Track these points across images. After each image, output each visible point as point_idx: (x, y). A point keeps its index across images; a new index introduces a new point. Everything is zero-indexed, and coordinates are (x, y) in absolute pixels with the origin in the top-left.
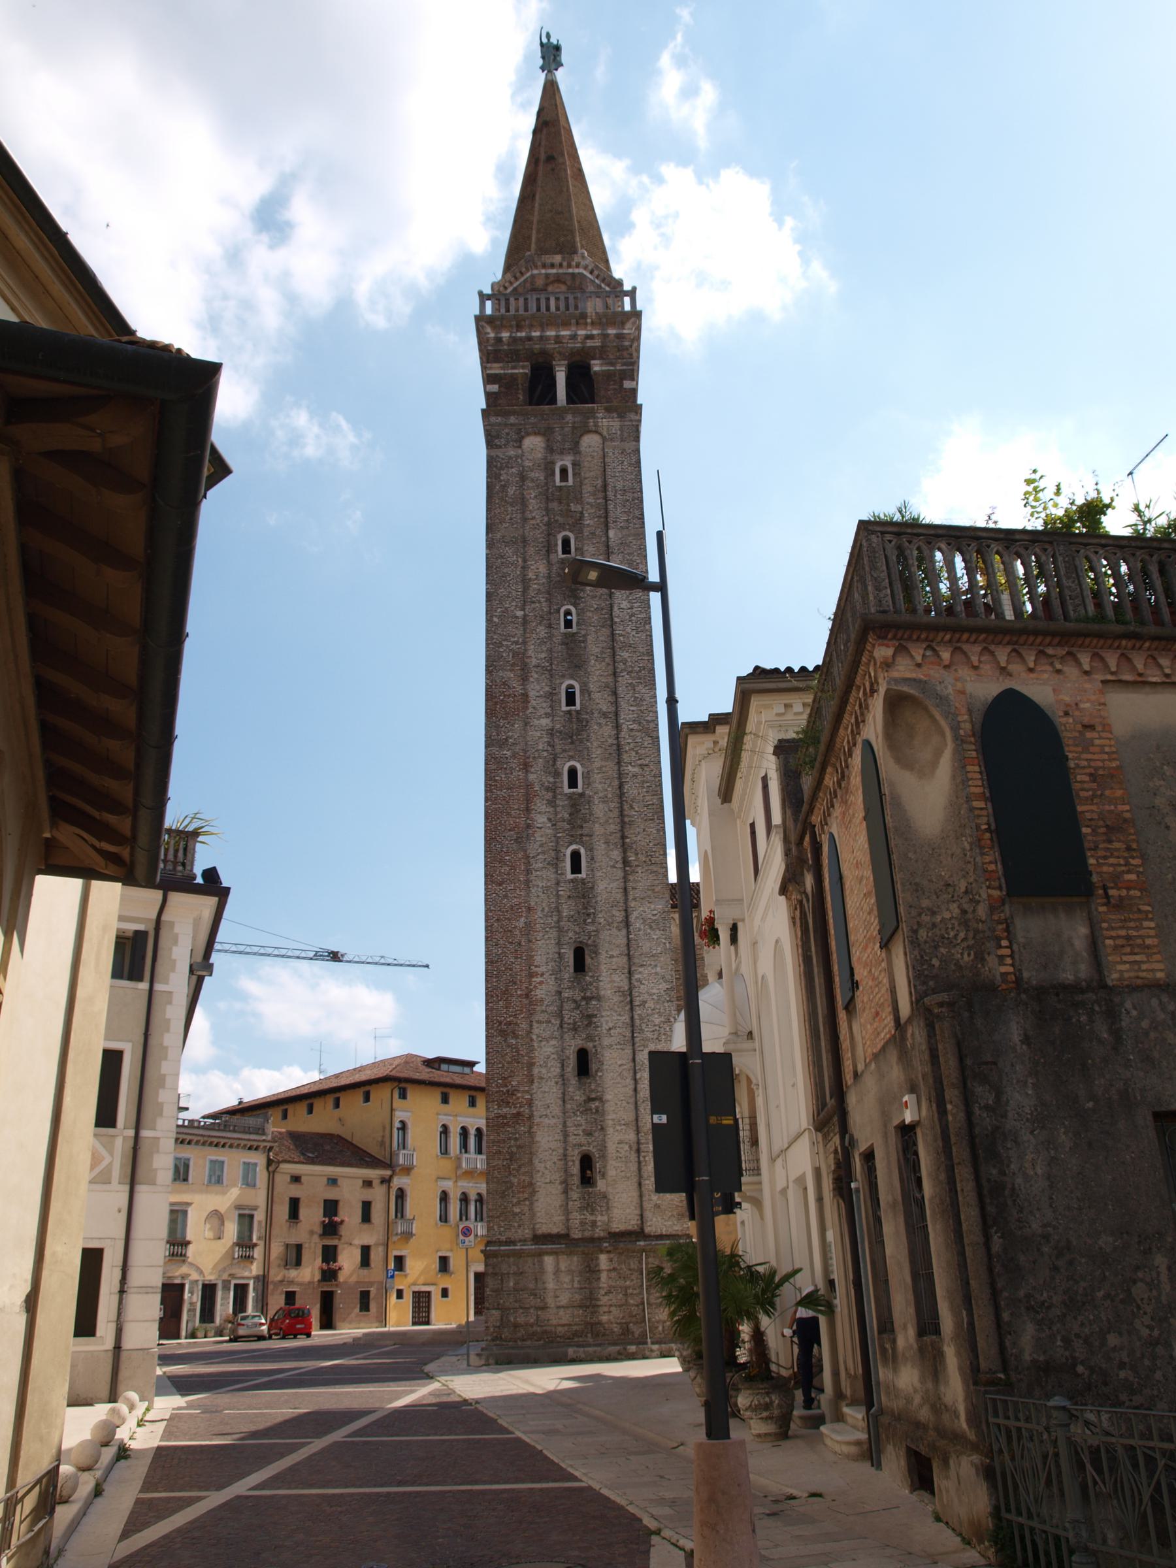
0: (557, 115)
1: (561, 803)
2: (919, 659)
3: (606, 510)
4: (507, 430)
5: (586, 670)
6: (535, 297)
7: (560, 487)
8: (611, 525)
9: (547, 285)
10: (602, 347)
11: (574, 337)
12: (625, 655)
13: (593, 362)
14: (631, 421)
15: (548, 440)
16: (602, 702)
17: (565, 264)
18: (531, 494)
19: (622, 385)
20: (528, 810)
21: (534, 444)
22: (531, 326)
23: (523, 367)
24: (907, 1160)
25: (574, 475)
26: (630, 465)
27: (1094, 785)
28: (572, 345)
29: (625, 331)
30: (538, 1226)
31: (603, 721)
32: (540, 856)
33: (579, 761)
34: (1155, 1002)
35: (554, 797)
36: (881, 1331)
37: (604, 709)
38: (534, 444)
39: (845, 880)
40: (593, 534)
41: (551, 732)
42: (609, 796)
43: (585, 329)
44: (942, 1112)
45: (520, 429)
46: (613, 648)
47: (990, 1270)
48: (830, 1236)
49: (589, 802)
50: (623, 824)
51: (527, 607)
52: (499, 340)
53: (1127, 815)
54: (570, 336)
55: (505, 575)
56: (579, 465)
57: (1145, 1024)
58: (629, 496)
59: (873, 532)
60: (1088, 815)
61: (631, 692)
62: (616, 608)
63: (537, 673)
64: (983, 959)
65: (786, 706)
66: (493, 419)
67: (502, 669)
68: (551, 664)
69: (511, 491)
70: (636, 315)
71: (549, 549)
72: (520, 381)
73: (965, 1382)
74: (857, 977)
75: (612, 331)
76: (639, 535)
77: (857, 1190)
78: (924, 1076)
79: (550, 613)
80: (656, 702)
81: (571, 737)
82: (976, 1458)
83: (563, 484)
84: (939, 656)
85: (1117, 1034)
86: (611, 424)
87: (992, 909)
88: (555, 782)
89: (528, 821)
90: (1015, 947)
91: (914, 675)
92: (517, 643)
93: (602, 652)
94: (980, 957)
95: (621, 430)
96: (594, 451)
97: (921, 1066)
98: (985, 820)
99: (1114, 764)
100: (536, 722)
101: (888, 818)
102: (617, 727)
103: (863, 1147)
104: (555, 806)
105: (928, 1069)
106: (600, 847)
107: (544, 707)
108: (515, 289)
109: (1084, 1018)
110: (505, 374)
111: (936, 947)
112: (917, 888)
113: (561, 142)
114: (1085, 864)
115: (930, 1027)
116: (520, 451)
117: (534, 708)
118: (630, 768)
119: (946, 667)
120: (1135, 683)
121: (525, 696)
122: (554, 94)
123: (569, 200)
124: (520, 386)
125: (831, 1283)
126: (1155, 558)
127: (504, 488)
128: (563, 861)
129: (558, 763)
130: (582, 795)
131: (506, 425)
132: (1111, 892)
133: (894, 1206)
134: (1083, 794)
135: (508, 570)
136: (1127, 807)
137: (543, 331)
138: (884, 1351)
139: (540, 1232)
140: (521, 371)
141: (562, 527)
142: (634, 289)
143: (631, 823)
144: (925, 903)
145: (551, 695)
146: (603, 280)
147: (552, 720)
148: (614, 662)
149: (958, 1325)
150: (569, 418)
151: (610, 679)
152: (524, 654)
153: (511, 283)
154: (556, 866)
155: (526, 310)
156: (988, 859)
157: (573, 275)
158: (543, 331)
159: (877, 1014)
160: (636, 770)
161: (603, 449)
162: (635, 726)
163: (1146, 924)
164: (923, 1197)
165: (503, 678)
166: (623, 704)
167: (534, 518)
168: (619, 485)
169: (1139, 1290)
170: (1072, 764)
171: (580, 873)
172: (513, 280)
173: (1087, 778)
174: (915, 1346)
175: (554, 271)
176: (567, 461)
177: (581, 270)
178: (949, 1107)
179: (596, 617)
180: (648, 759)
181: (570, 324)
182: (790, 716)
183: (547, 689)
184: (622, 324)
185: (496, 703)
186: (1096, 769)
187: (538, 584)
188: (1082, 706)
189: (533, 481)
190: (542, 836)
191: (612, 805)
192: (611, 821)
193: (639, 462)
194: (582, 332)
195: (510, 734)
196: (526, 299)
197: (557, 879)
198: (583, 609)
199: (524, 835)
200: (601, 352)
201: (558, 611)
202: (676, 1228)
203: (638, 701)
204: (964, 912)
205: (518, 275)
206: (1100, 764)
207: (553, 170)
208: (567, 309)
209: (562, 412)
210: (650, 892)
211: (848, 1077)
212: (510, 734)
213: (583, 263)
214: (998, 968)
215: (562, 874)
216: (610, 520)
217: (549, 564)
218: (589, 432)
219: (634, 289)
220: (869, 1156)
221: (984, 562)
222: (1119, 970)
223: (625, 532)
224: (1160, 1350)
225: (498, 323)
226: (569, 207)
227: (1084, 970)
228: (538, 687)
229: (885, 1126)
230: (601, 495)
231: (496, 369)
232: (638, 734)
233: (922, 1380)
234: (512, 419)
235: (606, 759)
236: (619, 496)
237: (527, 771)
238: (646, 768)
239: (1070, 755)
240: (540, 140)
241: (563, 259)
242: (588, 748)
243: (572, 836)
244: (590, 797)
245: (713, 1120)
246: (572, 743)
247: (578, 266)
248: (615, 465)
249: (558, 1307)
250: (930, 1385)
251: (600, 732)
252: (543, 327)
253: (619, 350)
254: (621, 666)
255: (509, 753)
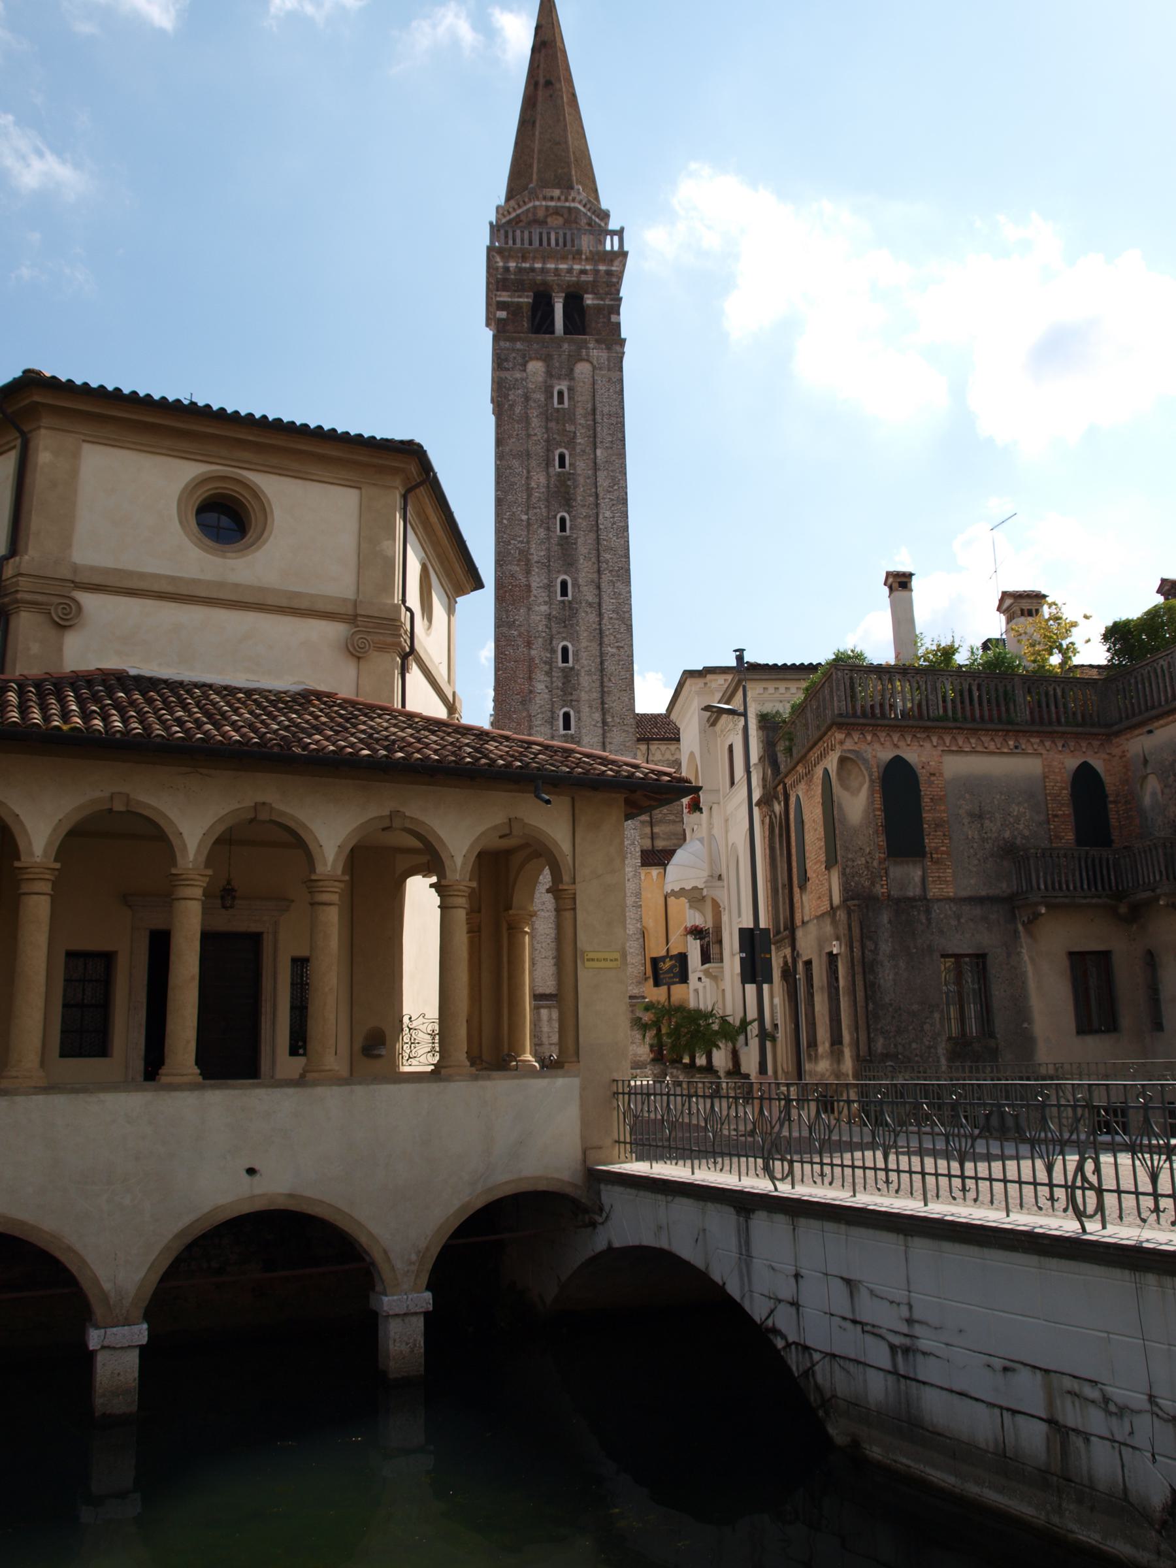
0: (554, 34)
1: (556, 675)
2: (856, 740)
3: (595, 430)
4: (514, 355)
5: (576, 567)
6: (538, 231)
7: (558, 409)
8: (598, 445)
9: (546, 217)
10: (594, 281)
11: (570, 271)
12: (608, 556)
13: (586, 296)
14: (617, 353)
15: (548, 366)
16: (589, 594)
17: (563, 198)
18: (534, 413)
19: (610, 319)
20: (530, 678)
21: (536, 367)
22: (534, 259)
23: (527, 297)
24: (830, 968)
25: (569, 398)
26: (615, 392)
27: (932, 804)
28: (569, 279)
29: (614, 268)
30: (535, 988)
31: (589, 610)
32: (539, 716)
33: (570, 642)
34: (947, 906)
35: (551, 669)
36: (809, 1046)
37: (590, 600)
38: (536, 367)
39: (805, 823)
40: (584, 451)
41: (549, 617)
42: (593, 670)
43: (580, 264)
44: (852, 951)
45: (525, 355)
46: (598, 550)
47: (867, 1017)
48: (777, 1001)
49: (577, 675)
50: (603, 693)
51: (530, 512)
52: (507, 269)
53: (945, 819)
54: (567, 269)
55: (514, 484)
56: (573, 390)
57: (942, 916)
58: (613, 420)
59: (839, 670)
60: (927, 819)
61: (611, 587)
62: (601, 517)
63: (538, 568)
64: (874, 885)
65: (765, 689)
66: (502, 344)
67: (510, 564)
68: (549, 561)
69: (518, 410)
70: (623, 254)
71: (548, 463)
72: (525, 310)
73: (853, 1061)
74: (808, 875)
75: (602, 268)
76: (620, 455)
77: (800, 979)
78: (844, 935)
79: (549, 518)
80: (630, 596)
81: (564, 622)
82: (856, 1090)
83: (560, 406)
84: (866, 738)
85: (929, 920)
86: (600, 354)
87: (880, 863)
88: (552, 658)
89: (531, 688)
90: (889, 881)
91: (853, 748)
92: (522, 542)
93: (589, 553)
94: (873, 884)
95: (609, 360)
96: (585, 378)
97: (842, 930)
98: (880, 821)
99: (942, 793)
100: (537, 608)
101: (835, 812)
102: (600, 615)
103: (805, 958)
104: (551, 677)
105: (846, 932)
106: (585, 710)
107: (543, 596)
108: (518, 216)
109: (916, 913)
110: (512, 303)
111: (853, 877)
112: (847, 849)
113: (558, 66)
114: (923, 842)
115: (849, 914)
116: (525, 375)
117: (535, 596)
118: (609, 649)
119: (869, 744)
120: (957, 751)
121: (529, 586)
122: (551, 12)
123: (565, 130)
124: (525, 315)
125: (776, 1026)
126: (976, 682)
127: (512, 406)
128: (558, 720)
129: (554, 642)
130: (572, 669)
131: (513, 350)
132: (934, 856)
133: (822, 988)
134: (926, 808)
135: (515, 480)
136: (945, 815)
137: (544, 263)
138: (809, 1056)
139: (537, 992)
140: (526, 300)
141: (559, 445)
142: (622, 229)
143: (609, 693)
144: (850, 856)
145: (549, 587)
146: (594, 213)
147: (550, 608)
148: (599, 562)
149: (852, 1039)
150: (566, 346)
151: (595, 575)
152: (527, 551)
153: (514, 210)
154: (552, 724)
155: (531, 244)
156: (880, 839)
157: (569, 209)
158: (544, 263)
159: (820, 898)
160: (614, 650)
161: (593, 377)
162: (614, 616)
163: (948, 871)
164: (838, 986)
165: (511, 571)
166: (605, 597)
167: (535, 435)
168: (606, 410)
169: (927, 1027)
170: (922, 793)
171: (570, 730)
172: (516, 207)
173: (929, 800)
174: (829, 1051)
175: (552, 204)
176: (563, 386)
177: (576, 205)
178: (855, 950)
179: (585, 523)
180: (623, 642)
181: (567, 258)
182: (766, 695)
183: (546, 581)
184: (611, 262)
185: (506, 591)
186: (933, 796)
187: (539, 493)
188: (931, 763)
189: (535, 401)
190: (541, 700)
191: (595, 677)
192: (594, 690)
193: (622, 390)
194: (577, 267)
195: (517, 617)
196: (530, 233)
197: (552, 733)
198: (574, 516)
199: (528, 698)
200: (593, 287)
201: (555, 517)
202: (634, 991)
203: (617, 595)
204: (867, 862)
205: (521, 203)
206: (936, 793)
207: (551, 96)
208: (565, 245)
209: (560, 340)
210: (622, 747)
211: (798, 922)
212: (517, 617)
213: (578, 198)
214: (880, 890)
215: (556, 730)
216: (598, 440)
217: (548, 476)
218: (582, 360)
219: (622, 229)
220: (808, 963)
221: (892, 685)
222: (934, 891)
223: (610, 451)
224: (932, 1050)
225: (507, 254)
226: (566, 137)
227: (918, 892)
228: (538, 580)
229: (820, 951)
230: (591, 417)
231: (504, 297)
232: (617, 622)
233: (831, 1065)
234: (519, 345)
235: (591, 641)
236: (605, 420)
237: (530, 648)
238: (621, 650)
239: (922, 789)
240: (539, 61)
241: (562, 193)
242: (577, 632)
243: (564, 701)
244: (578, 670)
245: (763, 956)
246: (565, 627)
247: (574, 200)
248: (603, 391)
249: (551, 1044)
250: (835, 1066)
251: (587, 618)
252: (544, 260)
253: (608, 286)
254: (604, 565)
255: (516, 633)
